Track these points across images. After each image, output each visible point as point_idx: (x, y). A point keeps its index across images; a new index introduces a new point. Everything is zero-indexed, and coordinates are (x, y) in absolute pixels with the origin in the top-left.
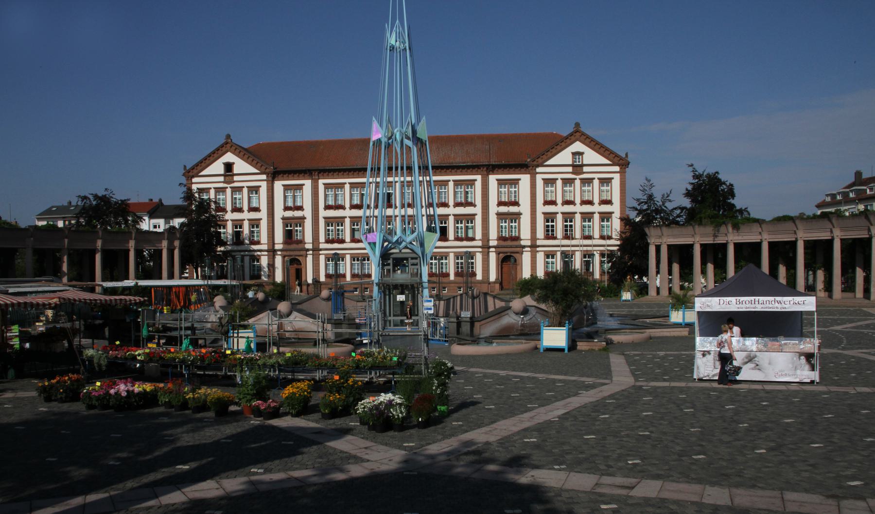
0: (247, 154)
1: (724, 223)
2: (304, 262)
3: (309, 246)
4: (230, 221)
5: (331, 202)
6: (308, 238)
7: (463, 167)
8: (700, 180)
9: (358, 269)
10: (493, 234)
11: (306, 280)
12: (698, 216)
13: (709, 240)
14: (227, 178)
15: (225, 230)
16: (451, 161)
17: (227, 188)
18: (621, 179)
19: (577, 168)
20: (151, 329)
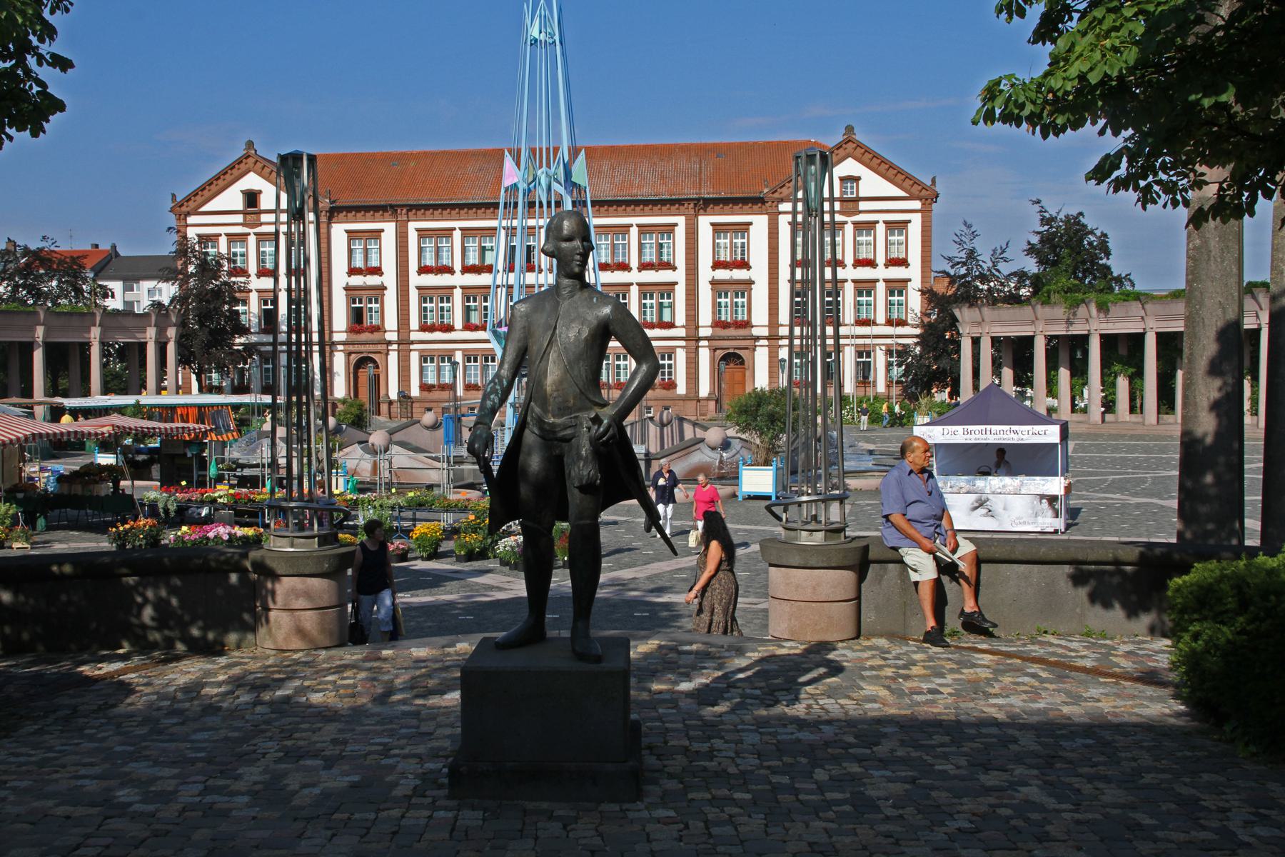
1: (1083, 301)
2: (384, 364)
3: (392, 336)
4: (254, 292)
5: (429, 261)
6: (391, 322)
7: (654, 203)
8: (1051, 227)
9: (476, 375)
10: (705, 317)
11: (387, 395)
12: (1045, 289)
13: (1060, 330)
14: (249, 217)
15: (246, 308)
16: (635, 192)
17: (249, 234)
20: (220, 466)
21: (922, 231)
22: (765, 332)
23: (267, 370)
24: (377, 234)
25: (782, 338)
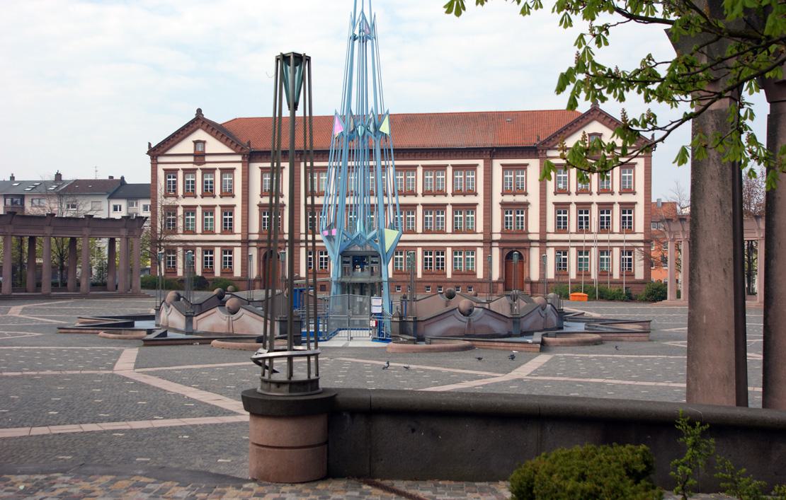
0: (219, 131)
10: (497, 226)
14: (197, 158)
18: (645, 164)
19: (199, 156)
21: (645, 170)
22: (537, 237)
23: (310, 259)
24: (474, 167)
25: (302, 241)
